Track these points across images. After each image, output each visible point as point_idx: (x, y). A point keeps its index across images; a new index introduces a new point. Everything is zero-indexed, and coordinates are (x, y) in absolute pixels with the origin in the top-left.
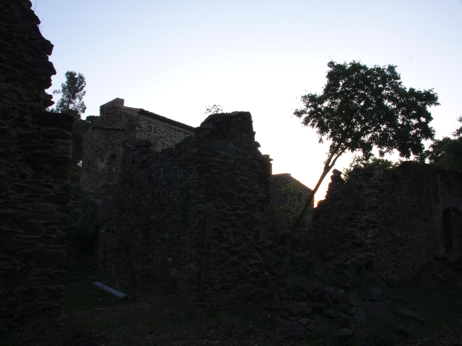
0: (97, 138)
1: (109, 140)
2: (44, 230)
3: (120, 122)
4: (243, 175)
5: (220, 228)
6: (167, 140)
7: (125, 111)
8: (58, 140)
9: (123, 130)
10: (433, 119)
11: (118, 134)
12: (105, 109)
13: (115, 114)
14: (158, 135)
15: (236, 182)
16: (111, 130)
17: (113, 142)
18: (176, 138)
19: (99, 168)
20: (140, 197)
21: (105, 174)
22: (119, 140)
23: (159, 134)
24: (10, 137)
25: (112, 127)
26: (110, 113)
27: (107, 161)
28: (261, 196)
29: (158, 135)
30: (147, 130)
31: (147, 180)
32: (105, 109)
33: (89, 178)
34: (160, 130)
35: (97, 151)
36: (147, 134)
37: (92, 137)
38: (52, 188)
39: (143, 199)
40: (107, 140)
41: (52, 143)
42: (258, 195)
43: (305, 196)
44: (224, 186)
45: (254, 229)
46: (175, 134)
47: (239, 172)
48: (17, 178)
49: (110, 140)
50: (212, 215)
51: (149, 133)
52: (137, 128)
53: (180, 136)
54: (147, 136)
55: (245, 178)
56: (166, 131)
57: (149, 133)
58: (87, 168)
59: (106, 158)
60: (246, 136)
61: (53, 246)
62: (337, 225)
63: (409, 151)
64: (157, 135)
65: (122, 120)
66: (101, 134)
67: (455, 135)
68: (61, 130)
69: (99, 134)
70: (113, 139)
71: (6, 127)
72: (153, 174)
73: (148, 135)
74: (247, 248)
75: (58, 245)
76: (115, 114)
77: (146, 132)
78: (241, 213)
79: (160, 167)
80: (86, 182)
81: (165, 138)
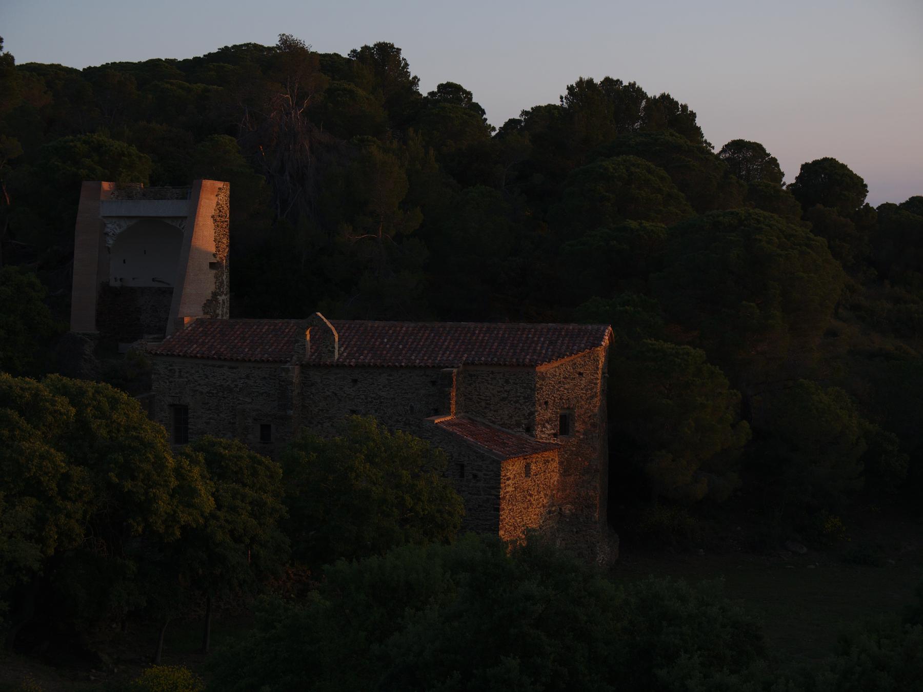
6: (199, 385)
10: (400, 50)
14: (186, 380)
18: (215, 378)
23: (187, 377)
29: (186, 380)
30: (168, 376)
34: (187, 372)
36: (167, 382)
43: (472, 468)
46: (214, 372)
51: (171, 379)
52: (153, 376)
53: (223, 374)
54: (168, 384)
56: (198, 372)
57: (171, 379)
63: (864, 206)
64: (182, 380)
67: (403, 58)
73: (170, 382)
77: (167, 379)
81: (197, 382)
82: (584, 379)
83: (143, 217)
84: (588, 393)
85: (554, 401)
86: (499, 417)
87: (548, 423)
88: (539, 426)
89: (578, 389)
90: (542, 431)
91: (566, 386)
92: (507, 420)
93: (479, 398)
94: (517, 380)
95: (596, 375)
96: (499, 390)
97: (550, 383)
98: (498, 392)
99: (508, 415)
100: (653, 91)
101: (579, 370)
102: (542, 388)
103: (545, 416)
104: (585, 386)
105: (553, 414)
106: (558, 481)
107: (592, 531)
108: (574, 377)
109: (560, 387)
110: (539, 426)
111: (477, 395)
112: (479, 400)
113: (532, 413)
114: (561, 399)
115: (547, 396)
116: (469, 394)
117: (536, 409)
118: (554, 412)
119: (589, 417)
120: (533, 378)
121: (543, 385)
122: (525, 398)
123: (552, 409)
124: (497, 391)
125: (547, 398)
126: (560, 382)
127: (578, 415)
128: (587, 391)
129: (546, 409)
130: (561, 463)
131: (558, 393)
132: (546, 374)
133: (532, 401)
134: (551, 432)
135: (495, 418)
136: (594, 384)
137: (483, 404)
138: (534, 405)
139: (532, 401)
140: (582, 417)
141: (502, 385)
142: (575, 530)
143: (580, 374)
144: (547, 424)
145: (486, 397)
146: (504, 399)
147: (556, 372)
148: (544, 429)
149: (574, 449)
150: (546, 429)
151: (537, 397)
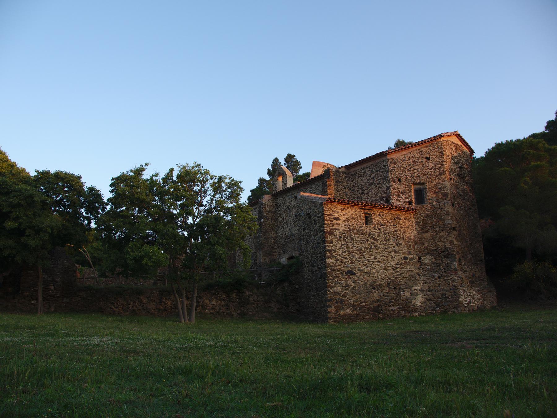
82: (431, 162)
83: (423, 142)
84: (436, 171)
85: (406, 178)
86: (370, 197)
87: (403, 194)
88: (395, 196)
89: (427, 169)
90: (397, 200)
91: (416, 167)
92: (374, 197)
93: (358, 188)
94: (378, 168)
95: (442, 159)
96: (368, 179)
97: (401, 166)
98: (368, 180)
99: (375, 194)
100: (53, 171)
101: (426, 156)
102: (394, 170)
103: (399, 189)
104: (433, 167)
105: (406, 187)
106: (415, 236)
107: (452, 276)
108: (422, 161)
109: (410, 169)
110: (395, 196)
111: (357, 187)
112: (358, 189)
113: (388, 188)
114: (412, 177)
115: (400, 175)
116: (353, 187)
117: (391, 184)
118: (407, 186)
119: (440, 188)
120: (386, 163)
121: (395, 167)
122: (383, 179)
123: (406, 184)
124: (367, 180)
125: (400, 176)
126: (410, 165)
127: (429, 188)
128: (435, 169)
129: (400, 184)
130: (417, 223)
131: (409, 172)
132: (397, 159)
133: (387, 179)
134: (405, 200)
135: (368, 199)
136: (441, 165)
137: (360, 191)
138: (389, 182)
139: (387, 179)
140: (434, 189)
141: (370, 174)
142: (436, 275)
143: (428, 159)
144: (402, 195)
145: (361, 186)
146: (372, 184)
147: (405, 158)
148: (399, 199)
149: (429, 212)
150: (401, 198)
151: (391, 176)
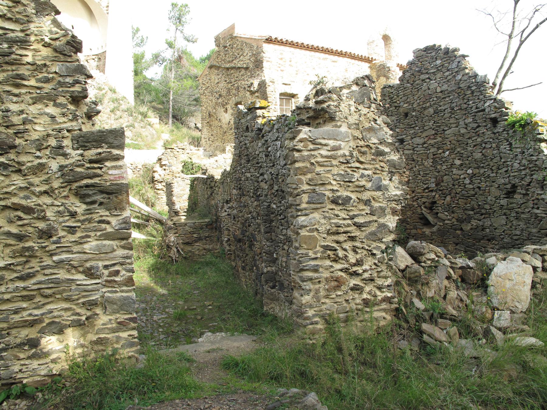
0: (217, 81)
1: (231, 83)
2: (106, 272)
3: (242, 57)
4: (365, 169)
5: (332, 245)
7: (247, 41)
8: (108, 164)
9: (247, 68)
11: (242, 73)
12: (221, 39)
13: (235, 46)
15: (353, 180)
16: (232, 68)
17: (236, 85)
19: (223, 121)
20: (258, 177)
21: (231, 129)
22: (243, 83)
24: (51, 172)
25: (233, 65)
26: (228, 45)
27: (232, 111)
28: (394, 193)
31: (264, 156)
32: (221, 39)
33: (212, 135)
35: (218, 99)
37: (210, 80)
38: (108, 223)
39: (262, 181)
40: (229, 83)
41: (101, 168)
42: (389, 194)
44: (335, 188)
45: (384, 240)
47: (358, 165)
48: (67, 218)
49: (233, 83)
50: (319, 229)
55: (366, 172)
58: (208, 122)
59: (230, 107)
60: (366, 113)
61: (118, 290)
62: (538, 208)
65: (245, 54)
66: (221, 75)
68: (109, 150)
69: (218, 75)
70: (236, 81)
71: (43, 161)
72: (269, 149)
74: (374, 267)
75: (125, 288)
76: (235, 46)
78: (362, 222)
79: (276, 140)
80: (209, 140)
